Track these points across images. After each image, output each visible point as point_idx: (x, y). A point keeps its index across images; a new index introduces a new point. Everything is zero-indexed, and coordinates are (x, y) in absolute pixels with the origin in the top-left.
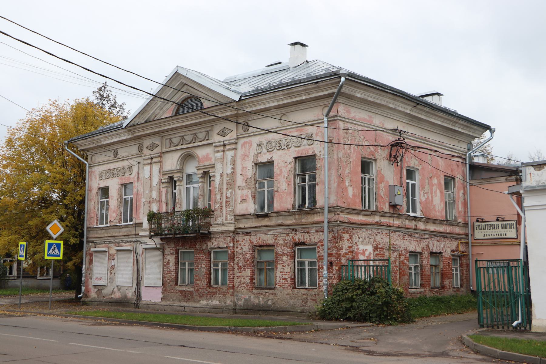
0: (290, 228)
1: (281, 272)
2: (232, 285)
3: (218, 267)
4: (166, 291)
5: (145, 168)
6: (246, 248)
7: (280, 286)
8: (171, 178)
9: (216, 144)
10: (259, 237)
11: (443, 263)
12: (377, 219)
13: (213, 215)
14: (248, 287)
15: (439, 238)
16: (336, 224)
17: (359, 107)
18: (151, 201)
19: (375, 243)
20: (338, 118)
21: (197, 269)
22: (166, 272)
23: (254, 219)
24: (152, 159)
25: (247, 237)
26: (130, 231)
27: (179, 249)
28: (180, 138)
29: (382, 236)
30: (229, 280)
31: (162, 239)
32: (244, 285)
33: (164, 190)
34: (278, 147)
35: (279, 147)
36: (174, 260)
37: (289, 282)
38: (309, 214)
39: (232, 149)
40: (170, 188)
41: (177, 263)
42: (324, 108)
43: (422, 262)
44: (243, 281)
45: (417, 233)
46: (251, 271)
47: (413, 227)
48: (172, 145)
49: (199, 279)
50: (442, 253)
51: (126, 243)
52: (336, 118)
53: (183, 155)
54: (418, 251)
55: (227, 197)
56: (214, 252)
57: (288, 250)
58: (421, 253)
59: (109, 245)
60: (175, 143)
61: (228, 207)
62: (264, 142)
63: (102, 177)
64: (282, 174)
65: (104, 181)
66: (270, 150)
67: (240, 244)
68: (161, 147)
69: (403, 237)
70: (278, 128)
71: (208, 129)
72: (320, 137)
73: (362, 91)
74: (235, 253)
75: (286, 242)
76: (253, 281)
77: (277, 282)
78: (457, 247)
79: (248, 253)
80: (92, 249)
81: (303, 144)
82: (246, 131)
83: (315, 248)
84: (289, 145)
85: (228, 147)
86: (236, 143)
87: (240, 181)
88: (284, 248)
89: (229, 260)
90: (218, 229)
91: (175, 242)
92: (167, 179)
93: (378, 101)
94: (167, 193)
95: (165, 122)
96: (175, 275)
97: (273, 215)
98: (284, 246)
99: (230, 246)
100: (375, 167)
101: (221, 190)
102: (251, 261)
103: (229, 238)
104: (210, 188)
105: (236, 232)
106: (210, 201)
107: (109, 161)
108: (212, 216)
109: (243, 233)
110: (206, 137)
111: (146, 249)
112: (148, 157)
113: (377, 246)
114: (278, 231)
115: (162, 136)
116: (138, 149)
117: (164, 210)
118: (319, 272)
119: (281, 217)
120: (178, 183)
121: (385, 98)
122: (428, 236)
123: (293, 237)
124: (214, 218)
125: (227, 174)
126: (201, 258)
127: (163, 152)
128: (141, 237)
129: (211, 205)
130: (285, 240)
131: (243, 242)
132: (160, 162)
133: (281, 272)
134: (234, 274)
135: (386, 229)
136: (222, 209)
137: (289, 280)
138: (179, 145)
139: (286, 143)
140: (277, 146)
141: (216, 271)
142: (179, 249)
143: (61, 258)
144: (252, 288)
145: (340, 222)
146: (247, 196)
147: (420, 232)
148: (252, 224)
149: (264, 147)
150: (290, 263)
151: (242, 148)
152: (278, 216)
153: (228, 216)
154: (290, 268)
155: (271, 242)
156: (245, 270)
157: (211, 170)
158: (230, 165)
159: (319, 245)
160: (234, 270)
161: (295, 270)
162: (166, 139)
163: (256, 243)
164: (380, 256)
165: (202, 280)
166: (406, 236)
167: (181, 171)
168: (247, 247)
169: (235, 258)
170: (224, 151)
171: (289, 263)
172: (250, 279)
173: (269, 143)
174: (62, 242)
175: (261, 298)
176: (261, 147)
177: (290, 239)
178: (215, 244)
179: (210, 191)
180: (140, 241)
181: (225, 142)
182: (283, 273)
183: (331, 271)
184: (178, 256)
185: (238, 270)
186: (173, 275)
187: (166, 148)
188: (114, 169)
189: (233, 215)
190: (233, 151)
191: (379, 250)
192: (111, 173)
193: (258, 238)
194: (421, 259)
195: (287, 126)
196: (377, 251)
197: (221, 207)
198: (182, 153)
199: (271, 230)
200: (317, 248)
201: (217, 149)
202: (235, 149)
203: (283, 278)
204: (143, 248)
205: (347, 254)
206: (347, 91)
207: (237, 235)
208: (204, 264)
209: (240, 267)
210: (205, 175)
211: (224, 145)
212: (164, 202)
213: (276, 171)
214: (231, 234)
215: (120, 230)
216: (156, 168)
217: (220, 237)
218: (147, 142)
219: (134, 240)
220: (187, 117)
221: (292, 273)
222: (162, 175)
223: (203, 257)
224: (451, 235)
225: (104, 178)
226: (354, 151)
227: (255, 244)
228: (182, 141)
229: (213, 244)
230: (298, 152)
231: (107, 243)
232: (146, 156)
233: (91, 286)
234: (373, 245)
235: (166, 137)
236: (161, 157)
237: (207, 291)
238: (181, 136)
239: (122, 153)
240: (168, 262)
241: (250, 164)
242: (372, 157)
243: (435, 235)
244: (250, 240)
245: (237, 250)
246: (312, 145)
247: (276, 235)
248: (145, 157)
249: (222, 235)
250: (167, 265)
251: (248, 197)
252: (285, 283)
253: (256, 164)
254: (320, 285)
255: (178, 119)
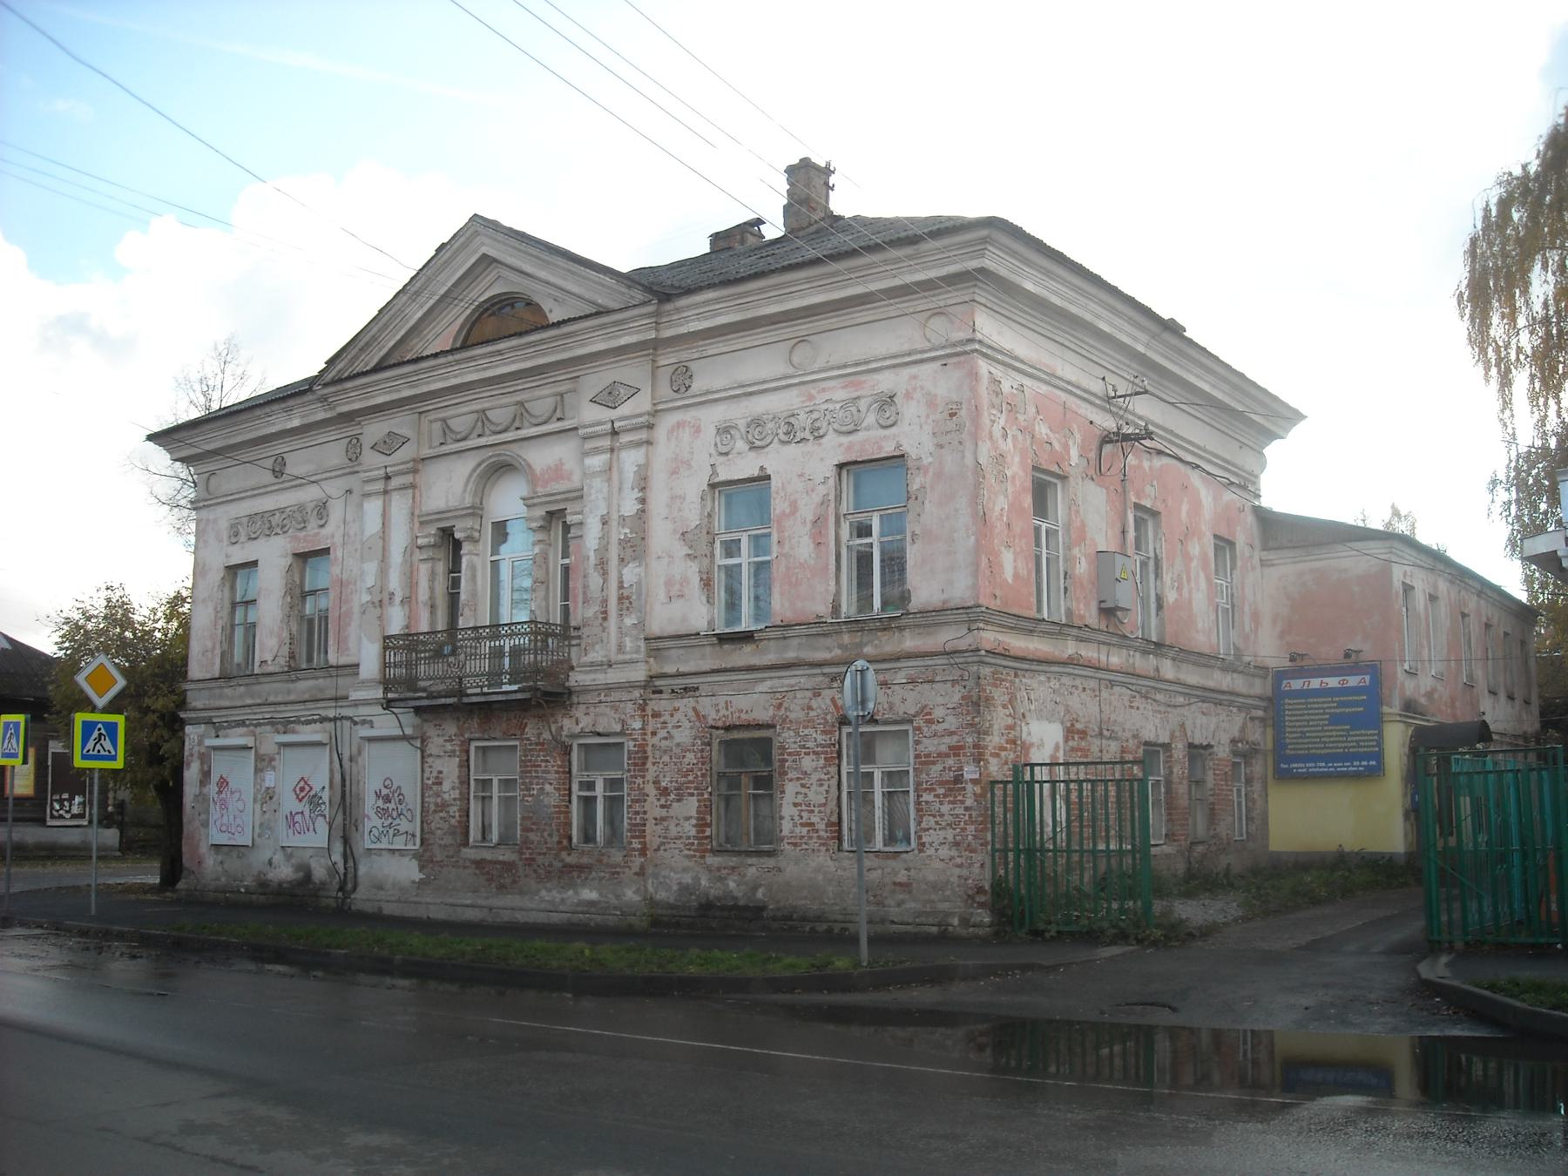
0: (824, 674)
1: (795, 805)
2: (639, 843)
3: (594, 790)
4: (432, 861)
5: (365, 505)
6: (684, 736)
7: (795, 845)
8: (447, 534)
9: (589, 430)
10: (726, 702)
11: (1214, 774)
12: (1070, 648)
13: (579, 637)
14: (689, 850)
15: (1205, 705)
16: (975, 659)
17: (1024, 322)
18: (384, 601)
19: (1067, 717)
20: (977, 346)
21: (530, 799)
22: (432, 807)
23: (708, 650)
24: (388, 478)
25: (685, 701)
26: (321, 690)
27: (471, 740)
28: (475, 416)
29: (1083, 695)
30: (630, 831)
31: (418, 710)
32: (679, 845)
33: (424, 569)
34: (785, 434)
35: (788, 433)
36: (456, 772)
37: (822, 833)
38: (885, 629)
39: (638, 444)
40: (441, 563)
41: (464, 781)
42: (930, 317)
43: (1171, 772)
44: (673, 831)
45: (1159, 690)
46: (699, 801)
47: (1152, 674)
48: (450, 436)
49: (534, 827)
50: (1212, 746)
51: (308, 722)
52: (968, 348)
53: (483, 466)
54: (1161, 741)
55: (621, 587)
56: (580, 745)
57: (820, 738)
58: (1167, 747)
59: (258, 730)
60: (460, 433)
61: (624, 612)
62: (739, 422)
63: (236, 534)
64: (798, 514)
65: (243, 548)
66: (758, 443)
67: (665, 723)
68: (416, 445)
69: (1131, 702)
70: (786, 377)
71: (562, 388)
72: (918, 402)
73: (1039, 276)
74: (649, 749)
75: (812, 714)
76: (704, 832)
77: (783, 834)
78: (1243, 729)
79: (689, 750)
80: (209, 742)
81: (864, 425)
82: (683, 389)
83: (906, 732)
84: (819, 429)
85: (625, 438)
86: (650, 427)
87: (661, 535)
88: (806, 732)
89: (629, 771)
90: (594, 680)
91: (458, 719)
92: (435, 535)
93: (1073, 309)
94: (433, 576)
95: (433, 368)
96: (460, 816)
97: (772, 635)
98: (805, 727)
99: (634, 729)
100: (1063, 498)
101: (602, 565)
102: (699, 773)
103: (630, 705)
104: (567, 561)
105: (651, 685)
106: (566, 597)
107: (259, 488)
108: (574, 642)
109: (673, 691)
110: (555, 411)
111: (371, 740)
112: (376, 473)
113: (1072, 725)
114: (786, 682)
115: (420, 413)
116: (347, 451)
117: (424, 627)
118: (918, 803)
119: (795, 642)
120: (466, 547)
121: (1091, 303)
122: (1181, 700)
123: (833, 700)
124: (583, 647)
125: (623, 518)
126: (540, 766)
127: (423, 459)
128: (356, 705)
129: (571, 610)
130: (810, 708)
131: (672, 715)
132: (413, 486)
133: (795, 805)
134: (645, 813)
135: (1092, 677)
136: (605, 619)
137: (822, 826)
138: (472, 436)
139: (809, 421)
140: (780, 431)
141: (589, 802)
142: (471, 740)
143: (119, 764)
144: (705, 851)
145: (987, 651)
146: (685, 581)
147: (1167, 687)
148: (701, 662)
149: (737, 436)
150: (826, 777)
151: (668, 440)
152: (785, 638)
153: (627, 639)
154: (827, 792)
155: (763, 716)
156: (679, 801)
157: (570, 508)
158: (633, 489)
159: (918, 722)
160: (645, 801)
161: (839, 798)
162: (431, 422)
163: (714, 720)
164: (1079, 753)
165: (544, 830)
166: (1135, 697)
167: (477, 511)
168: (687, 732)
169: (649, 765)
170: (612, 450)
171: (823, 777)
172: (694, 826)
173: (757, 422)
174: (120, 720)
175: (735, 881)
176: (729, 436)
177: (824, 707)
178: (585, 722)
179: (566, 570)
180: (350, 718)
181: (617, 425)
182: (804, 807)
183: (960, 798)
184: (468, 760)
185: (659, 800)
186: (454, 817)
187: (430, 448)
188: (272, 513)
189: (642, 637)
190: (643, 450)
191: (1076, 737)
192: (265, 525)
193: (722, 705)
194: (1167, 762)
195: (813, 373)
196: (1073, 739)
197: (603, 613)
198: (478, 460)
199: (763, 680)
200: (910, 732)
201: (589, 445)
202: (649, 443)
203: (804, 821)
204: (361, 738)
205: (1003, 749)
206: (1000, 268)
207: (653, 696)
208: (551, 784)
209: (665, 792)
210: (550, 522)
211: (615, 433)
212: (425, 604)
213: (778, 506)
214: (636, 693)
215: (291, 686)
216: (400, 506)
217: (600, 702)
218: (374, 430)
219: (331, 713)
220: (500, 353)
221: (833, 804)
222: (417, 525)
223: (547, 761)
224: (1232, 698)
225: (243, 538)
226: (1014, 446)
227: (711, 722)
228: (480, 424)
229: (577, 724)
230: (849, 448)
231: (251, 724)
232: (370, 471)
233: (204, 849)
234: (1062, 723)
235: (433, 416)
236: (415, 471)
237: (562, 861)
238: (477, 412)
239: (298, 464)
240: (437, 778)
241: (694, 485)
242: (1054, 468)
243: (1197, 696)
244: (694, 709)
245: (655, 740)
246: (894, 429)
247: (778, 695)
248: (367, 474)
249: (605, 696)
250: (435, 788)
251: (688, 583)
252: (811, 838)
253: (712, 486)
254: (924, 840)
255: (472, 359)
